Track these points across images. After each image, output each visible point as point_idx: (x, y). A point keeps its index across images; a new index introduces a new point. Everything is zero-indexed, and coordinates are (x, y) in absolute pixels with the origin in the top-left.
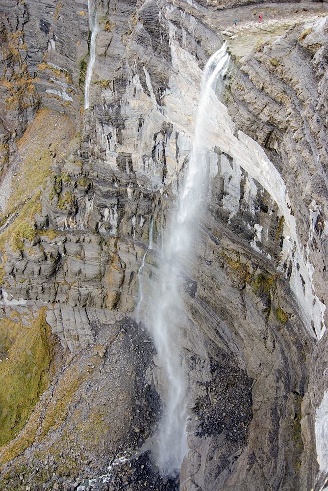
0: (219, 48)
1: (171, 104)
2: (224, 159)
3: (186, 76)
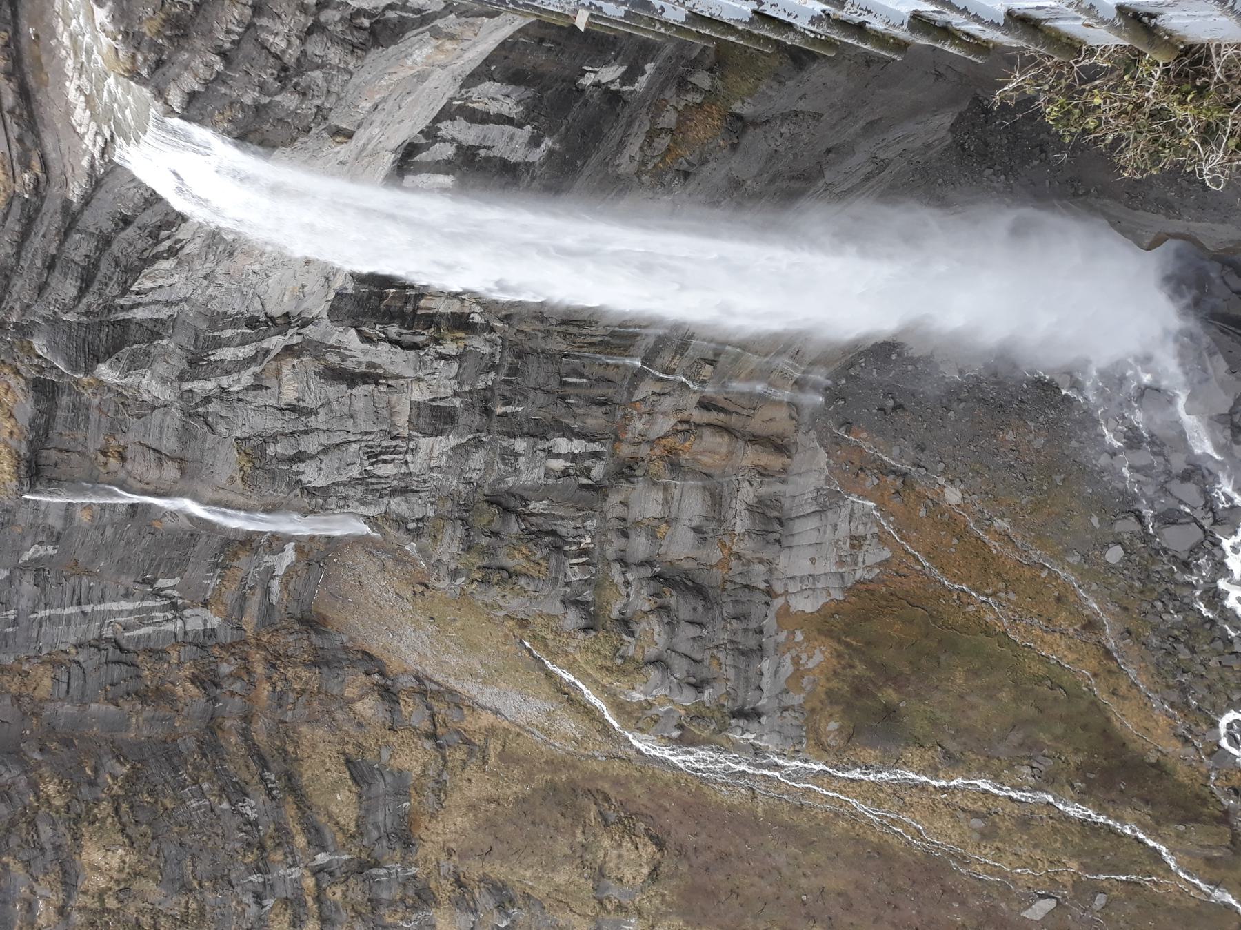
1: (286, 298)
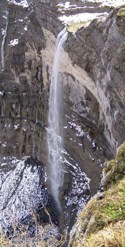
0: (63, 29)
1: (44, 54)
2: (70, 77)
3: (50, 41)
